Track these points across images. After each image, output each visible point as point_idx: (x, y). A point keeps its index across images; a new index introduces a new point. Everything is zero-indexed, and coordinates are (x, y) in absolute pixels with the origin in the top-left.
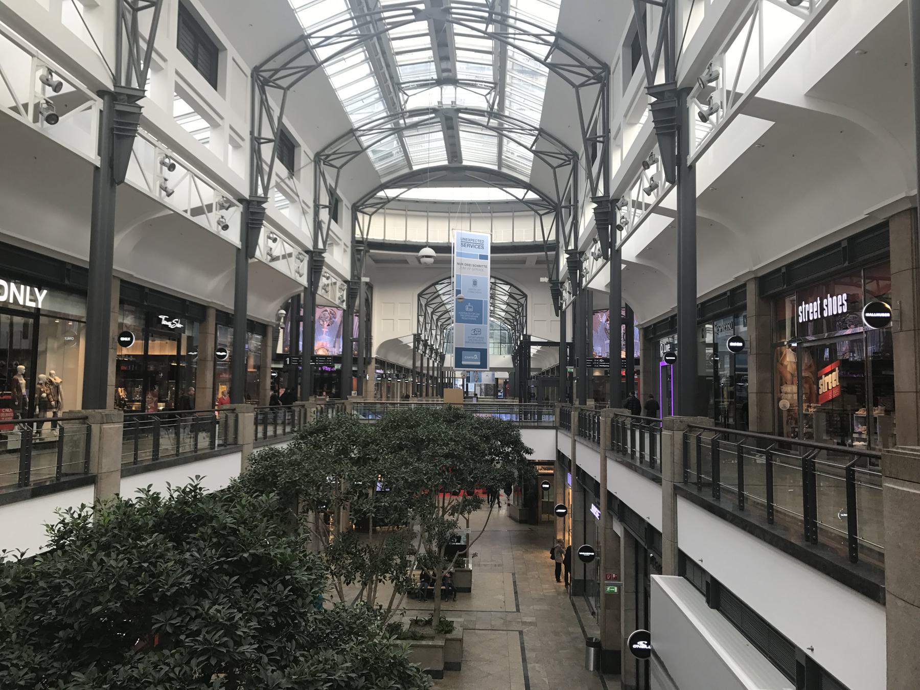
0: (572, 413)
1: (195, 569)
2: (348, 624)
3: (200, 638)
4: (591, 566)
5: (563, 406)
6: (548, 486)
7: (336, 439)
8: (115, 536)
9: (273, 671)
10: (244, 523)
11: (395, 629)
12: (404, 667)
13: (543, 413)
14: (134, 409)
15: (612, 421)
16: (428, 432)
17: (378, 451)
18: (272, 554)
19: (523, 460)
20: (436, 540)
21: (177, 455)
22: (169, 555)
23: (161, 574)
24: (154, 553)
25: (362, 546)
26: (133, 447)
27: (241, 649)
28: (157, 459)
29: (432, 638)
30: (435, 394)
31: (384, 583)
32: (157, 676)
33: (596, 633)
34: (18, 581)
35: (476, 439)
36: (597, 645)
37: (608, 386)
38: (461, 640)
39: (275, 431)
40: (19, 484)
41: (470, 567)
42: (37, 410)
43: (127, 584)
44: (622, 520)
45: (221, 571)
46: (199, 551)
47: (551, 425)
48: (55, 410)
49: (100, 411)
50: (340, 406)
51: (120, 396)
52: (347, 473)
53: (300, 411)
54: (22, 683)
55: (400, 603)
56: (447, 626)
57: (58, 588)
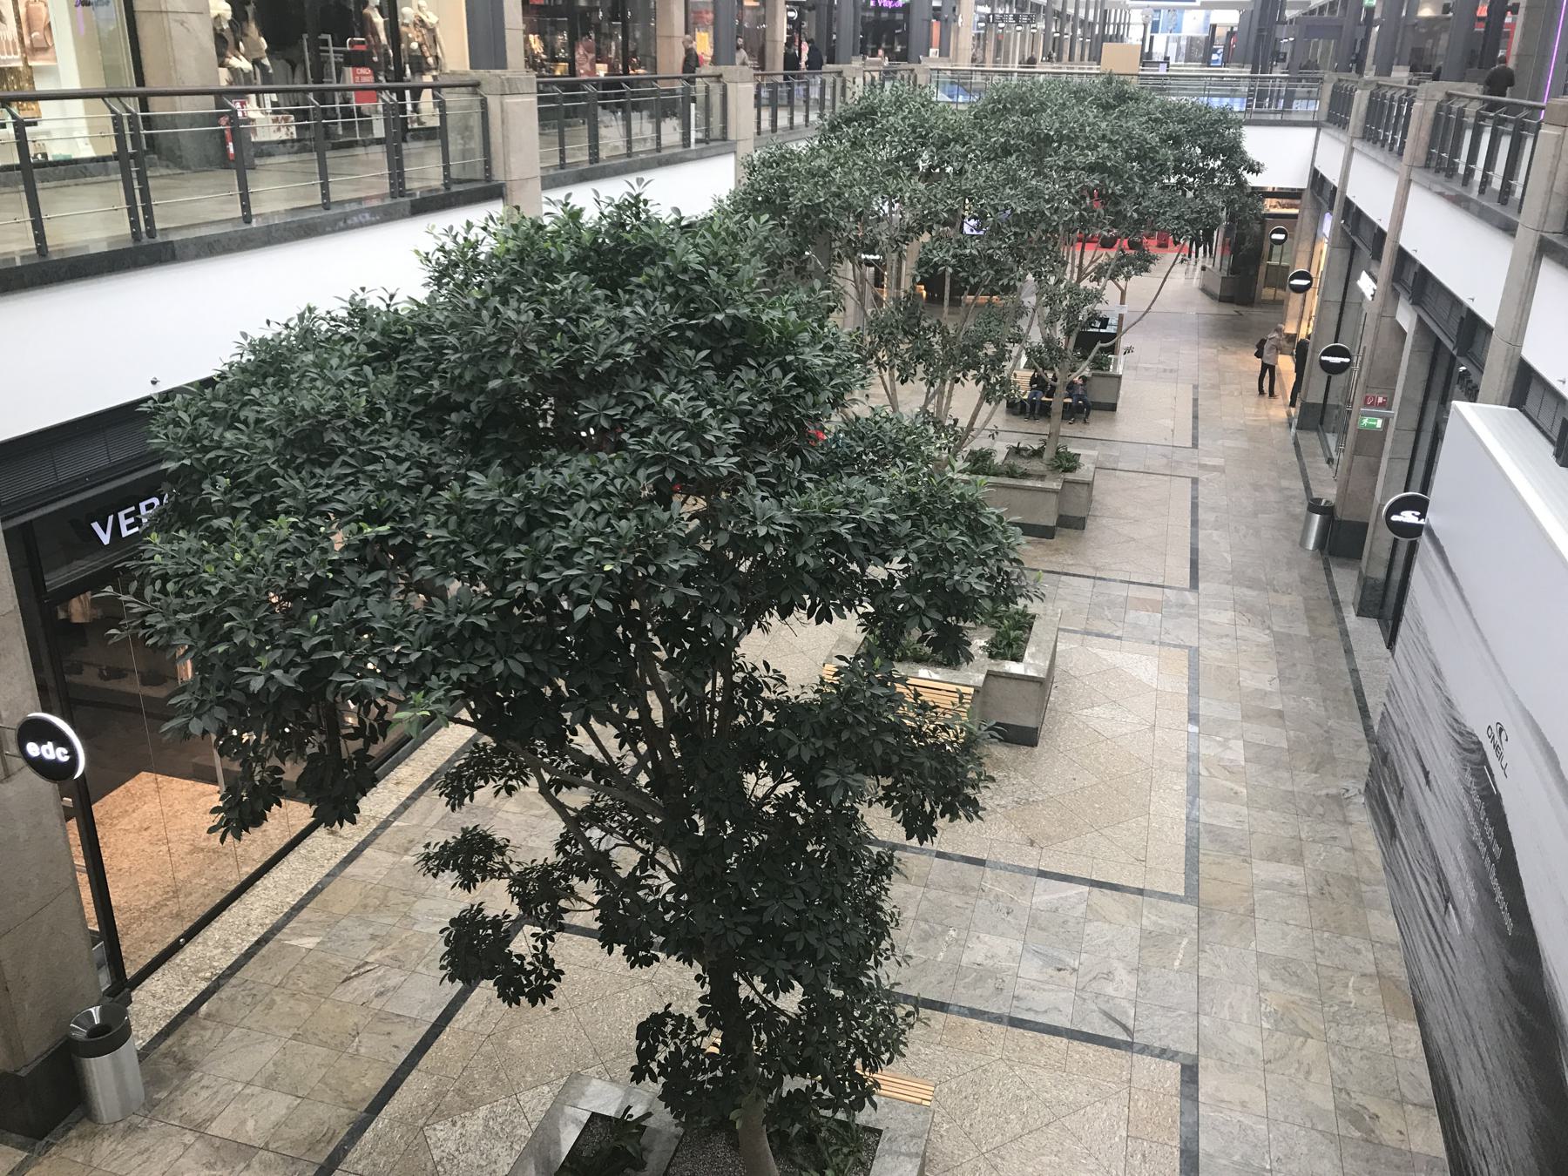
0: (1358, 92)
1: (640, 334)
2: (892, 441)
3: (650, 440)
4: (1339, 380)
5: (1340, 80)
6: (1281, 237)
7: (892, 131)
8: (515, 273)
9: (763, 498)
10: (717, 264)
11: (980, 462)
12: (976, 512)
13: (1297, 95)
14: (558, 73)
15: (1439, 108)
16: (1061, 122)
17: (965, 156)
18: (765, 318)
19: (1241, 184)
20: (1061, 321)
21: (629, 155)
22: (599, 309)
23: (586, 337)
24: (574, 304)
25: (929, 321)
26: (557, 139)
27: (713, 461)
28: (597, 161)
29: (1042, 477)
30: (1086, 57)
31: (963, 384)
32: (590, 488)
33: (1328, 493)
34: (389, 337)
35: (1153, 139)
36: (1327, 512)
37: (1444, 39)
38: (1089, 485)
39: (791, 119)
40: (392, 193)
41: (1120, 371)
42: (408, 71)
43: (536, 349)
44: (1417, 301)
45: (682, 340)
46: (646, 305)
47: (1310, 118)
48: (435, 73)
49: (498, 72)
50: (906, 76)
51: (532, 50)
52: (908, 195)
53: (834, 82)
54: (403, 482)
55: (989, 419)
56: (1068, 461)
57: (439, 349)
